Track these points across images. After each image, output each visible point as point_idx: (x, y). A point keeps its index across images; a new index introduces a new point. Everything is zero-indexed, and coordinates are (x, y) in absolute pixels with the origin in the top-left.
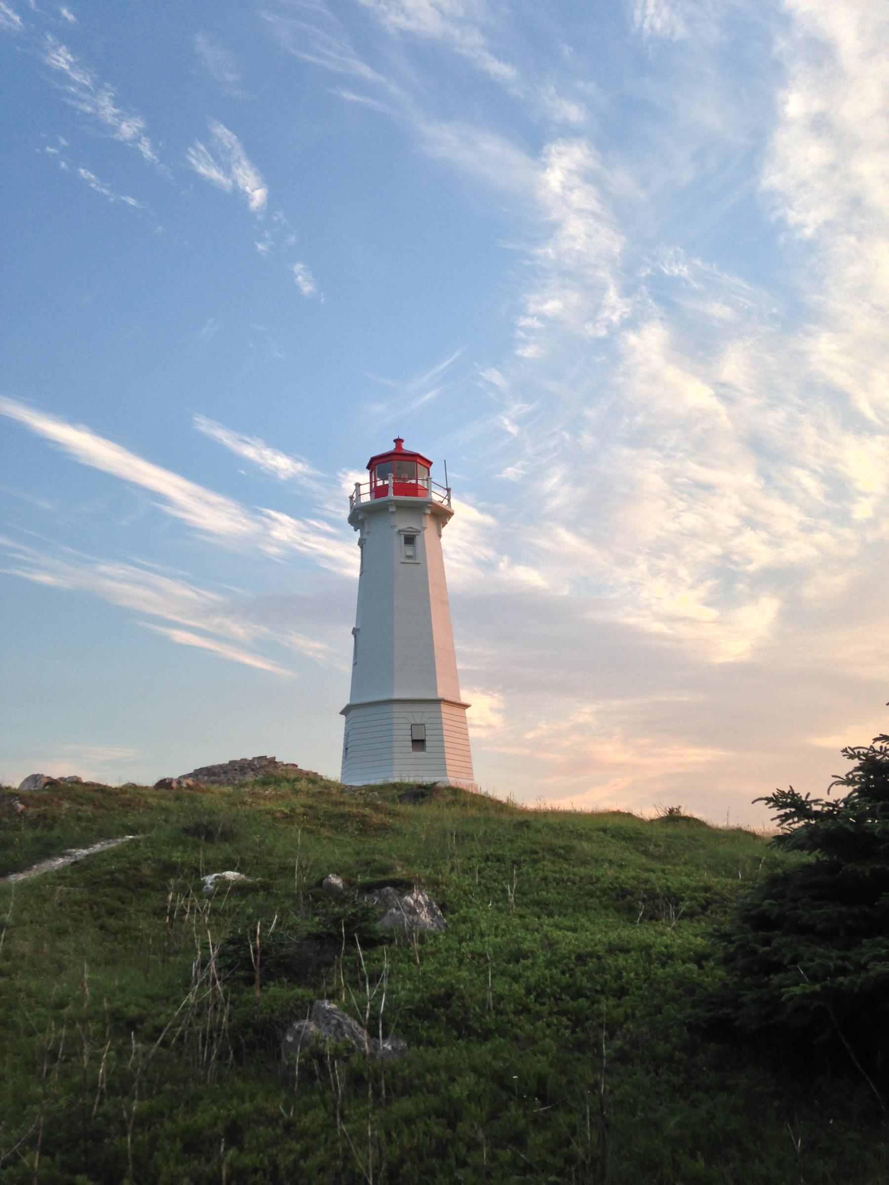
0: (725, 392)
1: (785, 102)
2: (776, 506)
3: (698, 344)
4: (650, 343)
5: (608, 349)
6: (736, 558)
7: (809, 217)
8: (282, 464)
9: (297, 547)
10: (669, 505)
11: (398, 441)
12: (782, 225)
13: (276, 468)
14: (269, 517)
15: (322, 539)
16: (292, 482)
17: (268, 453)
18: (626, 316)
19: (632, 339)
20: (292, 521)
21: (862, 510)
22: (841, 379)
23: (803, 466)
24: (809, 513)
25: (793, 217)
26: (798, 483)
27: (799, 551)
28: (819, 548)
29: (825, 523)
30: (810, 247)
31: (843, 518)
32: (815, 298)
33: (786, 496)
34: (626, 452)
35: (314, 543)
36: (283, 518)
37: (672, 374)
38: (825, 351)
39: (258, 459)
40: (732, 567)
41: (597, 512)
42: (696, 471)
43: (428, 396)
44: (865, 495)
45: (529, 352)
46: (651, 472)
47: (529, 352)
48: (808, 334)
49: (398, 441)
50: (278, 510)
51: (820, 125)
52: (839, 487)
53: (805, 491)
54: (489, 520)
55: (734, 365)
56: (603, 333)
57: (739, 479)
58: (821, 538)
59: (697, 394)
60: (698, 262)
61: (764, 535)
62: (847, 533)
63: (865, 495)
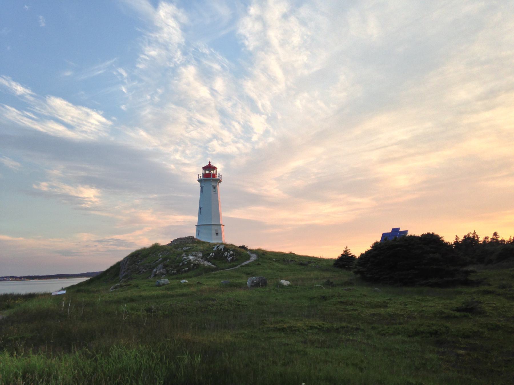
0: (213, 92)
1: (250, 10)
2: (225, 133)
3: (206, 75)
4: (190, 72)
5: (174, 71)
6: (210, 149)
7: (251, 44)
8: (20, 89)
9: (16, 122)
10: (187, 128)
11: (210, 162)
12: (243, 45)
13: (16, 90)
14: (6, 108)
15: (31, 121)
16: (22, 96)
17: (14, 84)
18: (183, 62)
19: (183, 70)
20: (16, 111)
21: (255, 138)
22: (253, 95)
23: (236, 121)
24: (236, 137)
25: (246, 43)
26: (234, 126)
27: (232, 149)
28: (238, 148)
29: (242, 141)
30: (251, 54)
31: (248, 139)
32: (250, 69)
33: (230, 131)
34: (173, 106)
35: (25, 121)
36: (13, 109)
37: (197, 84)
38: (249, 87)
39: (8, 86)
40: (207, 152)
41: (158, 126)
42: (199, 117)
43: (100, 72)
44: (256, 133)
45: (141, 66)
46: (182, 115)
47: (141, 66)
48: (245, 80)
49: (210, 162)
50: (12, 106)
51: (260, 18)
52: (247, 129)
53: (236, 129)
54: (110, 123)
55: (219, 84)
56: (172, 65)
57: (214, 122)
58: (240, 145)
59: (204, 92)
60: (212, 50)
61: (220, 142)
62: (248, 145)
63: (256, 133)
